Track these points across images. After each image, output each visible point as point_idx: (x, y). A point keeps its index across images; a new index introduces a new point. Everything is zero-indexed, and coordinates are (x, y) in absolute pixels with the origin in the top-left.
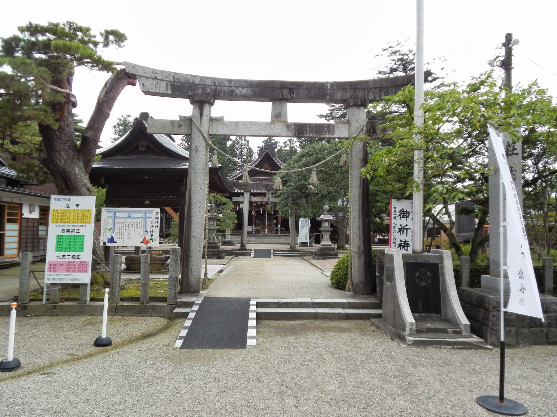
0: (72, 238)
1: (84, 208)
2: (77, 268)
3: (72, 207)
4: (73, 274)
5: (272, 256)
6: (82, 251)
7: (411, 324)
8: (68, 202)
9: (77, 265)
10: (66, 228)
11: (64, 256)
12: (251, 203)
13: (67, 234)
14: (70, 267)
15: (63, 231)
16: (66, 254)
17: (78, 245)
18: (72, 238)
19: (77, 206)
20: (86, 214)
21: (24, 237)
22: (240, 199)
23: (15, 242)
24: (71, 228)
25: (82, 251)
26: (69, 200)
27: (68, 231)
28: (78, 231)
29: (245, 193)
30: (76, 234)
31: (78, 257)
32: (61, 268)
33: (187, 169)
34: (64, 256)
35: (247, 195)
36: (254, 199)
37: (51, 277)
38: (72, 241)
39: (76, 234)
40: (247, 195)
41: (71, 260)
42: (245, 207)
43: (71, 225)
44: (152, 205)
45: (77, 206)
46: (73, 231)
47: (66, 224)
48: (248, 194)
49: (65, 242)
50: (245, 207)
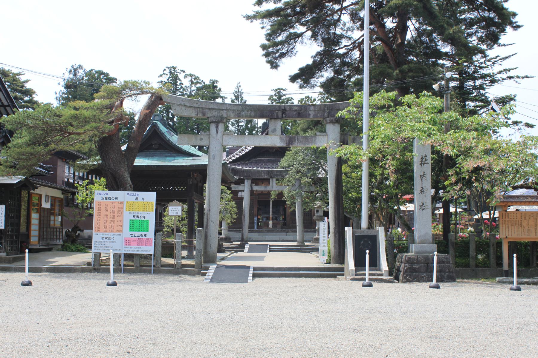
0: (141, 222)
1: (148, 201)
2: (144, 243)
3: (140, 200)
4: (142, 247)
5: (268, 251)
6: (148, 231)
7: (352, 270)
8: (137, 196)
9: (144, 241)
10: (136, 215)
11: (135, 234)
12: (252, 193)
13: (137, 219)
14: (140, 242)
15: (134, 217)
16: (137, 233)
17: (145, 227)
18: (141, 222)
19: (143, 199)
20: (150, 205)
21: (42, 219)
22: (240, 188)
23: (36, 225)
24: (139, 215)
25: (148, 231)
26: (138, 195)
27: (138, 217)
28: (144, 217)
29: (246, 181)
30: (143, 219)
31: (145, 235)
32: (134, 242)
33: (205, 166)
34: (135, 234)
35: (247, 183)
36: (256, 188)
37: (127, 249)
38: (141, 224)
39: (143, 219)
40: (247, 183)
41: (140, 237)
42: (245, 195)
43: (140, 212)
44: (152, 191)
45: (143, 199)
46: (141, 217)
47: (136, 212)
48: (250, 181)
49: (136, 224)
50: (245, 195)
